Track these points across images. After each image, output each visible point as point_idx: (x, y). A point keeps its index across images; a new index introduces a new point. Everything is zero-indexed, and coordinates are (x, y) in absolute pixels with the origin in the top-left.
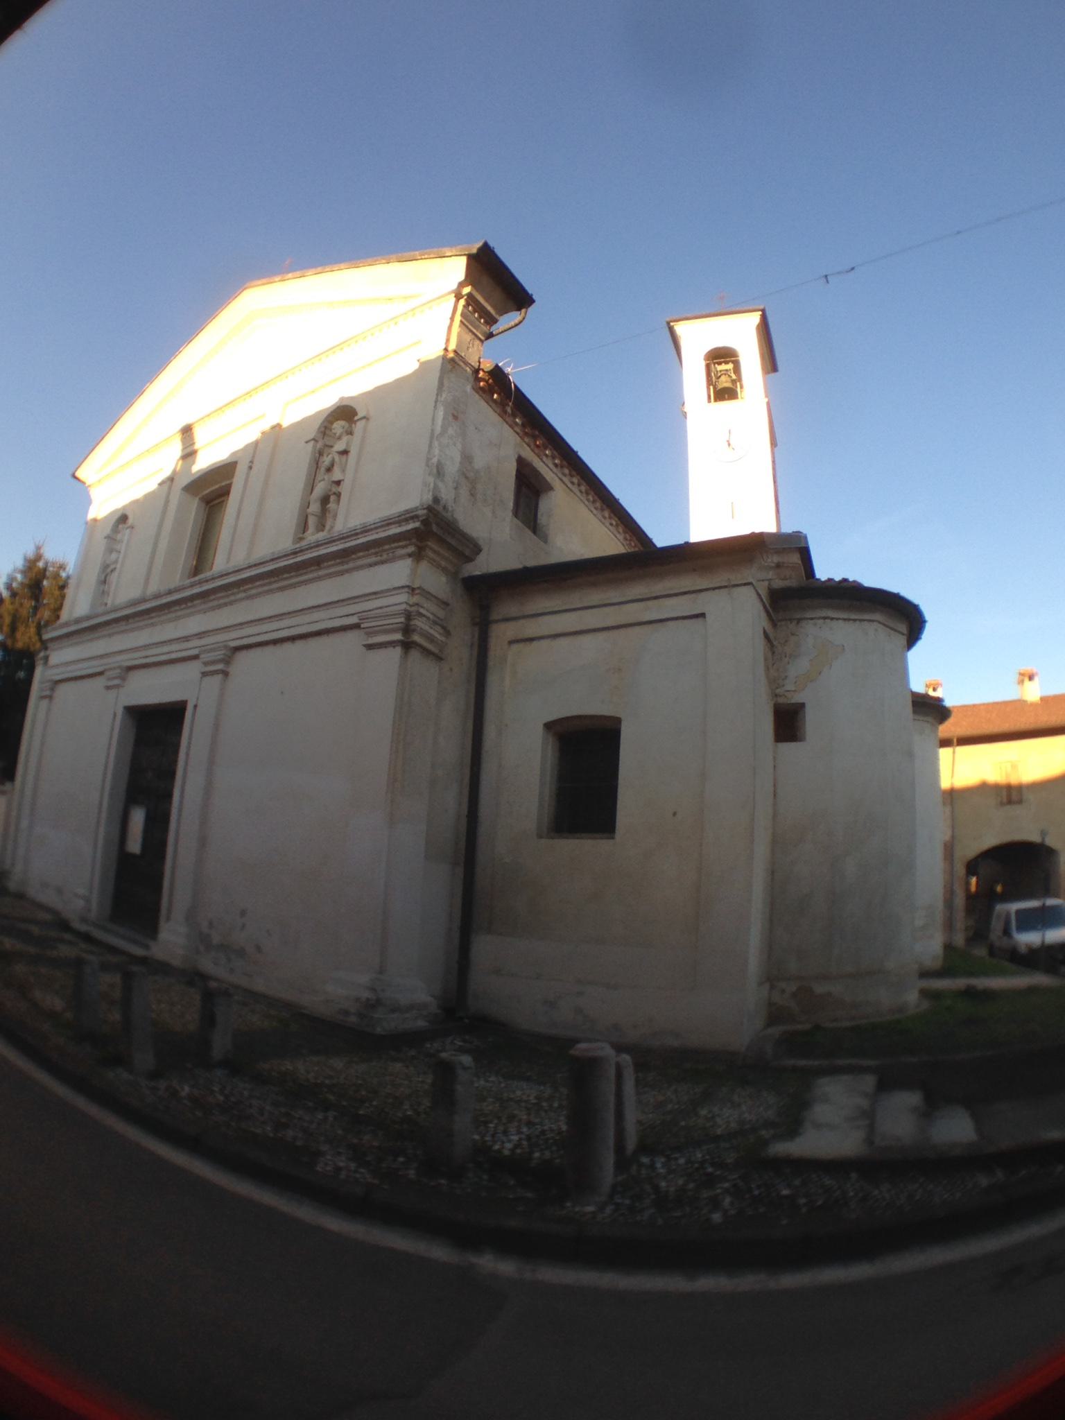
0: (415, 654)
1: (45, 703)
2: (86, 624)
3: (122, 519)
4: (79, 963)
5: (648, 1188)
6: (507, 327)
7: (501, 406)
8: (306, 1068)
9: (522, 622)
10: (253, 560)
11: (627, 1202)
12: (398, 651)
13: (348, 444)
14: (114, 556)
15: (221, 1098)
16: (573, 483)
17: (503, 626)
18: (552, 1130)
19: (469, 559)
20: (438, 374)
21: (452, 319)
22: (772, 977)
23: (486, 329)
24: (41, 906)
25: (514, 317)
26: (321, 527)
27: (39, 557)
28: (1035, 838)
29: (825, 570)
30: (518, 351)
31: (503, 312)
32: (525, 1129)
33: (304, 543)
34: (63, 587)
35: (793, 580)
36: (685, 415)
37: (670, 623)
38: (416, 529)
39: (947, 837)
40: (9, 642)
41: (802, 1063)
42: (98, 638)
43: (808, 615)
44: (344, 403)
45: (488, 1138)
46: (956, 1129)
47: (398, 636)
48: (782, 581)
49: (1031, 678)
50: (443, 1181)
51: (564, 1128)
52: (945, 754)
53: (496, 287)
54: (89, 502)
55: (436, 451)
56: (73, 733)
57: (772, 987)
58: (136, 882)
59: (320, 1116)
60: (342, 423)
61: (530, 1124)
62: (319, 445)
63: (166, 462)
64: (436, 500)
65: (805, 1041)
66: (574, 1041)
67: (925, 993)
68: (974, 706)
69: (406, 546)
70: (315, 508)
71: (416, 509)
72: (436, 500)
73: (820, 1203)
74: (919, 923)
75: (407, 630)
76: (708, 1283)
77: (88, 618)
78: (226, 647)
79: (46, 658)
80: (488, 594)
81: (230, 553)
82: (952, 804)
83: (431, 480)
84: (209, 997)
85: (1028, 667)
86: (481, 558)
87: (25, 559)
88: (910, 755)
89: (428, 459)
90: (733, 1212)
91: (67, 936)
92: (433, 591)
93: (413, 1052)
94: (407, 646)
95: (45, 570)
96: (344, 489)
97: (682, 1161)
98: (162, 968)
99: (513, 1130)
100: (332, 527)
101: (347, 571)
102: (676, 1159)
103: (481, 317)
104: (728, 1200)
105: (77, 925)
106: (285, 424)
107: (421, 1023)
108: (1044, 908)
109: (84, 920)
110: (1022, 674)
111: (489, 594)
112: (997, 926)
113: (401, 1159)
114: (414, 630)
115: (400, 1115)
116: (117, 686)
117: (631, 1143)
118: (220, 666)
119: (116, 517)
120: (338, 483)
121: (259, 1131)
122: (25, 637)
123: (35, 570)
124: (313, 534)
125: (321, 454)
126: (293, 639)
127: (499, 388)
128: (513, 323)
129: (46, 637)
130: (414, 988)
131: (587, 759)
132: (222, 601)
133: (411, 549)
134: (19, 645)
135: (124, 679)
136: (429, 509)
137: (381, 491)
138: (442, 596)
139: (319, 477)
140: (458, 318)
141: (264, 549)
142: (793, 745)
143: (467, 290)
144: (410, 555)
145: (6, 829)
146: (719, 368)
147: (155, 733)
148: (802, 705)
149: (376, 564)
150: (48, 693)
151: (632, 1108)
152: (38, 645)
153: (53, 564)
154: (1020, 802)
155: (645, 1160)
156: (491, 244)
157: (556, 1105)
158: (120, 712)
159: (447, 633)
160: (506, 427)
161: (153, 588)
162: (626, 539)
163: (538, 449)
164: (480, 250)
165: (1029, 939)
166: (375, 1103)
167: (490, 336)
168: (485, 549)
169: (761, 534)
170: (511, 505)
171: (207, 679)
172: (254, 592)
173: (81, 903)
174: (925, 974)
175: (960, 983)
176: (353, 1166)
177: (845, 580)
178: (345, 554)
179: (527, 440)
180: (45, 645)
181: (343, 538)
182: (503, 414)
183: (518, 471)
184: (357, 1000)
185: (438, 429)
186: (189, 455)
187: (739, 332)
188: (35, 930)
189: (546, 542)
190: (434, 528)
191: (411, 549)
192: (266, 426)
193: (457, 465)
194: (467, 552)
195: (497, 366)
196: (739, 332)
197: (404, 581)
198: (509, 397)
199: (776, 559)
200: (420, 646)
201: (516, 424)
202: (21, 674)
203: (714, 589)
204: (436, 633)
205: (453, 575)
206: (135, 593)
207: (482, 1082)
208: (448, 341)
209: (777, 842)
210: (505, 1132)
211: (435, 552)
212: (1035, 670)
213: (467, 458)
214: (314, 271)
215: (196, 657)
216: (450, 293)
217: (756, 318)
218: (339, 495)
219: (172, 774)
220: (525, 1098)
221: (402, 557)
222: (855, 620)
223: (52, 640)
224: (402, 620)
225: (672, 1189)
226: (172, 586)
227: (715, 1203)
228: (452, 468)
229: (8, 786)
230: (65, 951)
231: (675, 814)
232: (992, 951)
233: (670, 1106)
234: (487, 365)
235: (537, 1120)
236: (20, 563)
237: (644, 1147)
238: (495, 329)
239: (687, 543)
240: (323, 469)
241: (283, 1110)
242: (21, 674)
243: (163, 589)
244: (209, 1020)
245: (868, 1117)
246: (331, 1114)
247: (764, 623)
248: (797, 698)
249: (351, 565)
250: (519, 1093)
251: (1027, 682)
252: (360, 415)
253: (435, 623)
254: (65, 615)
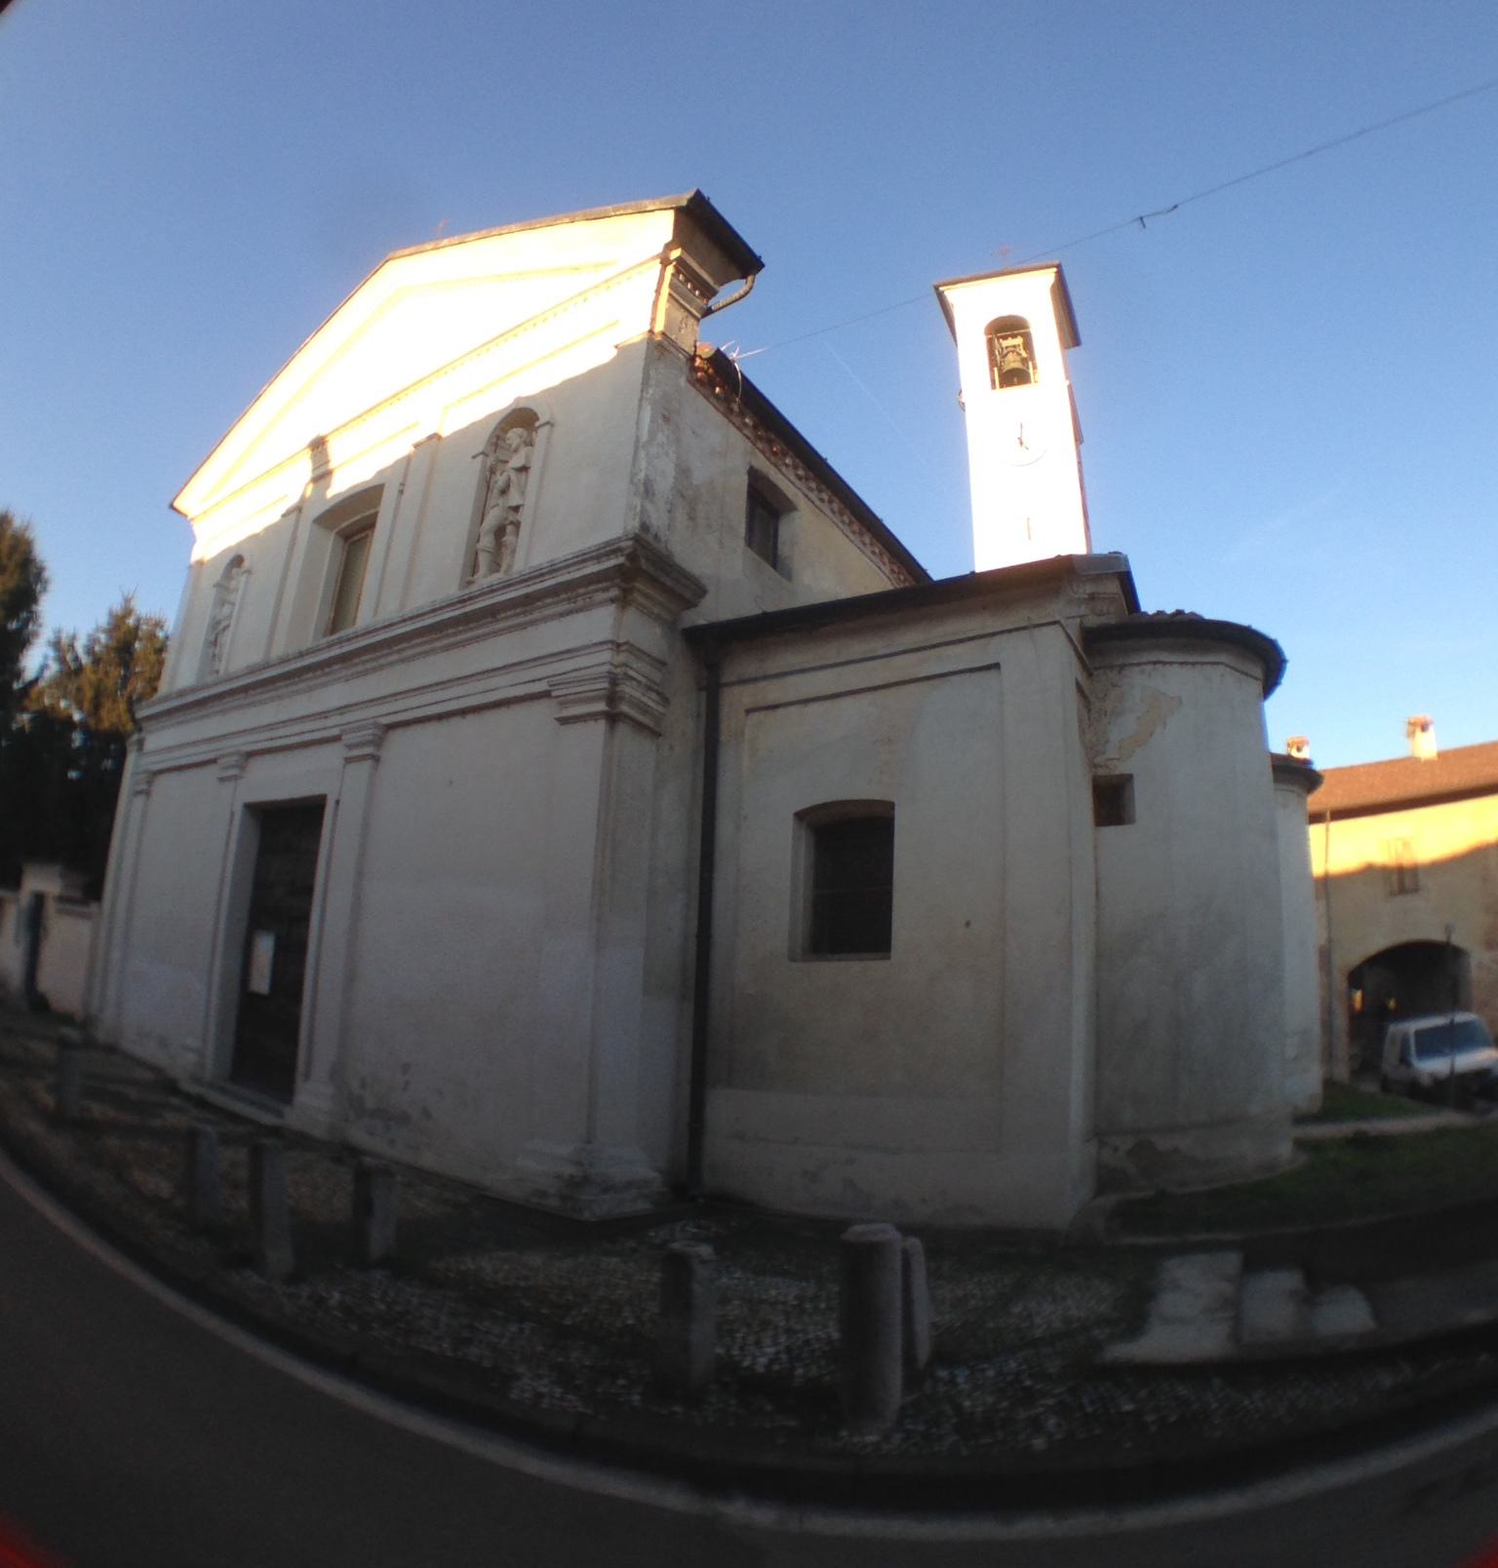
0: (623, 729)
1: (140, 801)
2: (190, 698)
3: (236, 561)
4: (192, 1136)
5: (948, 1409)
7: (725, 404)
8: (491, 1266)
9: (763, 684)
10: (408, 612)
11: (921, 1428)
12: (601, 726)
13: (527, 457)
14: (226, 609)
15: (382, 1307)
17: (736, 690)
18: (818, 1339)
19: (690, 604)
20: (641, 363)
21: (658, 292)
22: (1100, 1132)
23: (701, 303)
25: (737, 287)
26: (495, 566)
27: (128, 612)
28: (1438, 936)
29: (1153, 600)
30: (745, 331)
32: (782, 1339)
33: (474, 588)
34: (160, 650)
36: (962, 406)
37: (955, 679)
38: (620, 566)
39: (1323, 941)
40: (92, 722)
41: (1144, 1240)
42: (207, 716)
45: (735, 1352)
46: (1347, 1315)
47: (601, 706)
48: (1095, 615)
49: (1424, 728)
50: (677, 1409)
51: (836, 1336)
52: (1315, 831)
53: (713, 249)
55: (643, 464)
56: (175, 837)
58: (265, 1029)
59: (513, 1328)
60: (520, 430)
61: (789, 1331)
62: (490, 460)
63: (293, 485)
64: (645, 527)
65: (1149, 1208)
66: (843, 1225)
67: (1300, 1144)
69: (605, 590)
70: (487, 541)
71: (619, 539)
72: (645, 527)
73: (1173, 1418)
74: (1291, 1053)
75: (612, 698)
76: (1031, 1527)
77: (193, 690)
79: (141, 743)
80: (717, 650)
81: (378, 604)
83: (637, 502)
84: (364, 1177)
85: (1420, 715)
86: (707, 603)
87: (111, 614)
88: (1272, 835)
89: (633, 475)
90: (1059, 1436)
91: (175, 1101)
92: (645, 647)
94: (613, 718)
95: (137, 628)
96: (525, 517)
97: (991, 1373)
98: (300, 1140)
100: (510, 566)
101: (532, 623)
102: (983, 1370)
103: (695, 288)
106: (445, 433)
107: (642, 1206)
108: (1452, 1027)
109: (197, 1080)
110: (1412, 724)
111: (718, 650)
112: (1391, 1054)
113: (621, 1382)
114: (621, 699)
116: (235, 778)
117: (923, 1351)
118: (369, 750)
119: (227, 561)
120: (516, 509)
121: (434, 1349)
122: (112, 715)
123: (124, 629)
125: (492, 471)
126: (463, 712)
127: (720, 377)
129: (140, 714)
130: (633, 1161)
131: (851, 851)
134: (106, 725)
135: (242, 767)
136: (637, 539)
137: (573, 516)
138: (656, 653)
139: (491, 502)
140: (666, 290)
141: (420, 600)
142: (1119, 829)
143: (676, 253)
144: (612, 601)
146: (1005, 343)
148: (1129, 778)
150: (144, 787)
151: (923, 1306)
152: (130, 726)
153: (148, 621)
154: (1416, 890)
155: (943, 1373)
157: (823, 1306)
158: (239, 810)
159: (665, 701)
160: (733, 429)
161: (278, 651)
163: (775, 457)
164: (690, 201)
165: (1435, 1066)
167: (708, 312)
168: (711, 589)
169: (1070, 558)
170: (742, 529)
171: (352, 766)
172: (410, 653)
173: (191, 1057)
174: (1300, 1119)
175: (1347, 1128)
176: (558, 1391)
177: (1179, 613)
178: (528, 602)
181: (525, 580)
182: (728, 413)
183: (751, 486)
184: (559, 1177)
185: (644, 437)
186: (322, 476)
187: (1029, 295)
189: (789, 578)
191: (614, 592)
192: (421, 435)
193: (671, 480)
194: (688, 595)
196: (1029, 295)
199: (1089, 588)
200: (632, 720)
202: (108, 763)
203: (1010, 631)
204: (651, 701)
205: (670, 626)
206: (255, 657)
207: (725, 1280)
208: (653, 320)
209: (1102, 957)
210: (758, 1343)
211: (646, 596)
212: (1429, 717)
213: (683, 471)
214: (476, 235)
215: (337, 739)
216: (653, 258)
217: (1048, 277)
218: (517, 525)
219: (309, 890)
221: (601, 603)
222: (1194, 664)
224: (606, 685)
227: (1036, 1425)
228: (664, 485)
230: (172, 1119)
231: (968, 924)
232: (1386, 1085)
234: (706, 351)
235: (799, 1327)
236: (103, 620)
237: (943, 1356)
238: (713, 303)
239: (973, 573)
240: (496, 491)
242: (108, 763)
243: (292, 650)
245: (1233, 1307)
246: (527, 1326)
248: (1122, 769)
249: (536, 615)
250: (773, 1292)
251: (1419, 734)
252: (542, 420)
253: (649, 689)
254: (164, 687)
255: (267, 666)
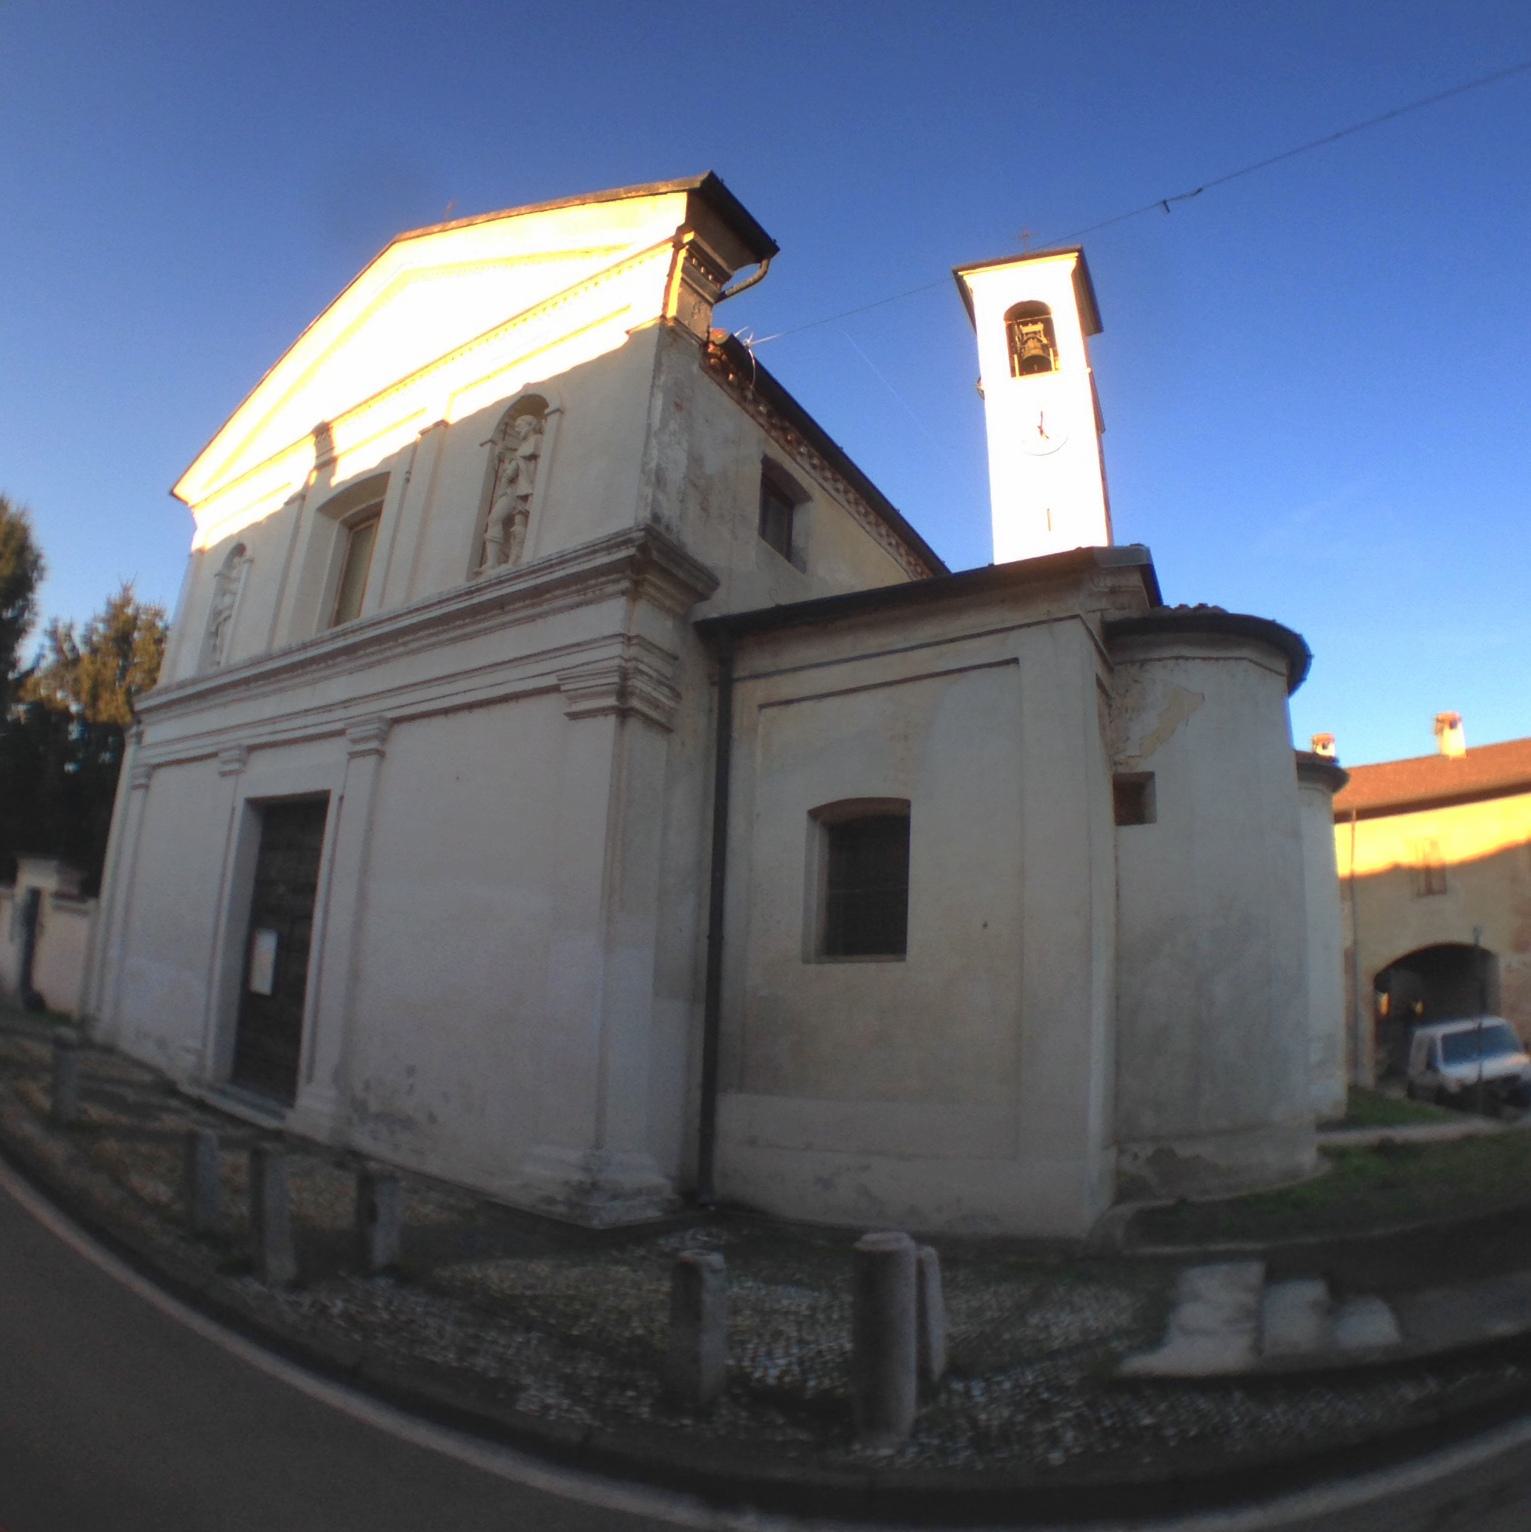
0: (634, 725)
1: (139, 794)
2: (190, 690)
3: (237, 550)
4: (192, 1139)
5: (962, 1421)
6: (743, 284)
7: (738, 392)
8: (498, 1275)
9: (777, 678)
10: (417, 600)
12: (612, 719)
13: (537, 447)
14: (227, 600)
16: (837, 490)
17: (750, 684)
18: (831, 1349)
19: (703, 597)
20: (653, 350)
21: (670, 276)
22: (1120, 1138)
23: (715, 287)
24: (140, 1064)
25: (752, 271)
26: (504, 557)
27: (126, 601)
28: (1465, 938)
29: (1174, 594)
31: (738, 264)
32: (795, 1350)
33: (482, 580)
34: (159, 641)
35: (1134, 609)
36: (981, 394)
37: (973, 674)
38: (630, 557)
39: (1348, 943)
40: (89, 713)
43: (1155, 654)
44: (530, 392)
45: (746, 1363)
46: (1372, 1328)
47: (612, 701)
48: (1113, 605)
49: (1453, 725)
51: (848, 1346)
52: (1341, 831)
54: (193, 527)
55: (655, 453)
56: (175, 834)
57: (1121, 1152)
58: (266, 1032)
60: (528, 418)
61: (801, 1342)
62: (498, 449)
63: (297, 472)
64: (656, 518)
65: (1170, 1220)
67: (1325, 1152)
68: (1378, 766)
69: (617, 581)
70: (495, 532)
72: (656, 518)
73: (1192, 1433)
74: (1314, 1058)
75: (623, 693)
77: (194, 682)
78: (381, 719)
79: (139, 736)
80: (730, 643)
81: (386, 591)
82: (1352, 898)
83: (649, 491)
84: (367, 1182)
86: (720, 595)
87: (109, 603)
89: (644, 464)
90: (1077, 1450)
91: (174, 1103)
93: (641, 1252)
94: (624, 714)
95: (135, 618)
96: (534, 507)
97: (1007, 1385)
98: (304, 1145)
99: (779, 1351)
100: (518, 557)
101: (540, 616)
102: (999, 1383)
104: (1069, 1436)
105: (187, 1088)
106: (452, 419)
107: (653, 1213)
108: (1479, 1032)
110: (1438, 720)
112: (1417, 1058)
113: (630, 1393)
114: (632, 694)
115: (627, 1334)
117: (938, 1364)
118: (374, 745)
120: (525, 498)
121: (438, 1359)
123: (122, 618)
124: (493, 567)
125: (501, 460)
126: (470, 707)
127: (734, 365)
128: (751, 280)
129: (139, 706)
130: (643, 1169)
131: (866, 865)
132: (374, 658)
133: (625, 584)
134: (103, 717)
135: (243, 762)
136: (648, 530)
137: (581, 508)
140: (678, 274)
141: (429, 588)
143: (689, 237)
144: (623, 593)
145: (89, 959)
146: (1026, 329)
147: (289, 829)
148: (1150, 776)
149: (579, 605)
150: (143, 781)
151: (939, 1316)
152: (128, 718)
153: (147, 610)
154: (1443, 891)
155: (958, 1386)
156: (720, 175)
157: (835, 1316)
158: (240, 806)
159: (677, 696)
160: (746, 416)
161: (281, 642)
162: (909, 563)
164: (704, 183)
165: (1460, 1072)
166: (593, 1320)
167: (722, 297)
169: (1090, 550)
170: (756, 520)
171: (358, 762)
174: (1325, 1125)
176: (565, 1403)
177: (1202, 606)
178: (537, 593)
179: (774, 433)
180: (137, 718)
181: (534, 571)
182: (741, 400)
184: (566, 1183)
185: (656, 423)
187: (1050, 280)
188: (131, 1096)
189: (804, 570)
190: (655, 555)
191: (625, 584)
194: (700, 587)
195: (732, 337)
196: (1050, 280)
197: (618, 629)
198: (749, 377)
199: (1109, 582)
201: (760, 413)
202: (106, 757)
203: (1029, 625)
204: (662, 696)
206: (257, 648)
207: (736, 1289)
208: (665, 305)
210: (769, 1354)
211: (659, 589)
212: (1458, 715)
213: (695, 459)
215: (341, 733)
216: (667, 241)
217: (1070, 261)
218: (526, 515)
219: (312, 888)
220: (793, 1308)
222: (1217, 659)
223: (148, 710)
224: (616, 679)
225: (995, 1423)
226: (308, 639)
227: (1053, 1439)
228: (676, 475)
229: (91, 904)
230: (170, 1122)
231: (985, 925)
232: (1412, 1092)
233: (989, 1314)
234: (719, 336)
235: (811, 1338)
236: (101, 609)
238: (727, 288)
240: (504, 480)
241: (471, 1331)
242: (106, 757)
244: (367, 1212)
245: (1256, 1317)
246: (535, 1335)
247: (1098, 667)
248: (1143, 766)
249: (546, 607)
250: (785, 1302)
251: (1447, 732)
253: (660, 683)
254: (163, 679)
255: (270, 658)
